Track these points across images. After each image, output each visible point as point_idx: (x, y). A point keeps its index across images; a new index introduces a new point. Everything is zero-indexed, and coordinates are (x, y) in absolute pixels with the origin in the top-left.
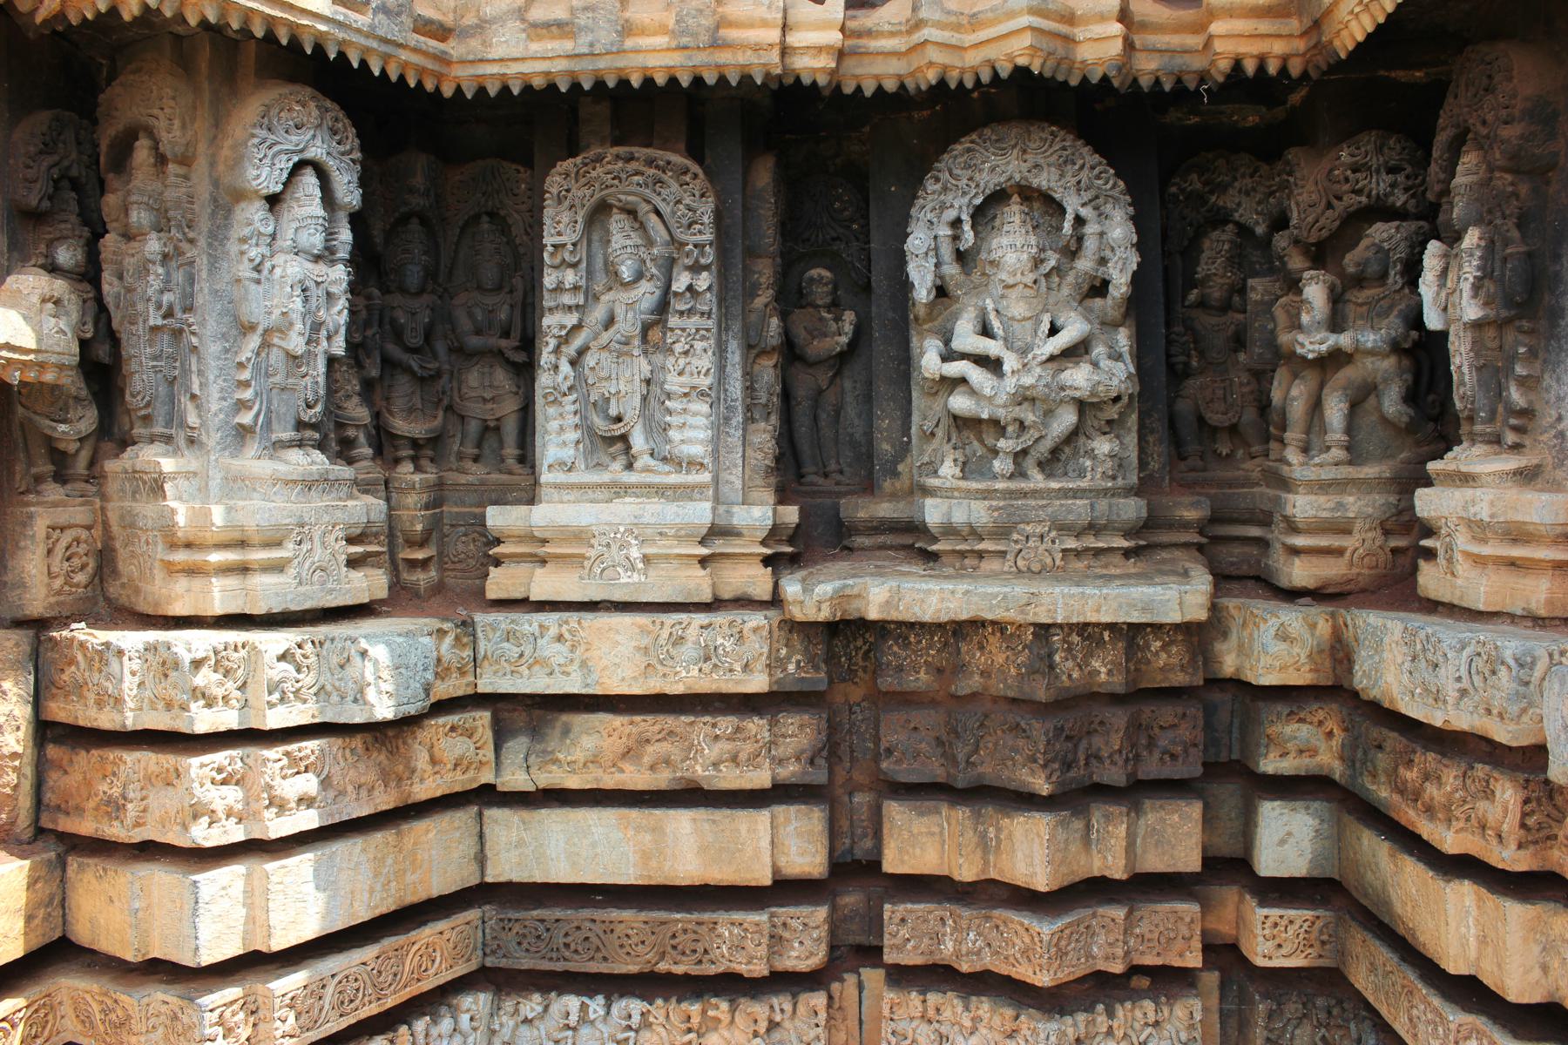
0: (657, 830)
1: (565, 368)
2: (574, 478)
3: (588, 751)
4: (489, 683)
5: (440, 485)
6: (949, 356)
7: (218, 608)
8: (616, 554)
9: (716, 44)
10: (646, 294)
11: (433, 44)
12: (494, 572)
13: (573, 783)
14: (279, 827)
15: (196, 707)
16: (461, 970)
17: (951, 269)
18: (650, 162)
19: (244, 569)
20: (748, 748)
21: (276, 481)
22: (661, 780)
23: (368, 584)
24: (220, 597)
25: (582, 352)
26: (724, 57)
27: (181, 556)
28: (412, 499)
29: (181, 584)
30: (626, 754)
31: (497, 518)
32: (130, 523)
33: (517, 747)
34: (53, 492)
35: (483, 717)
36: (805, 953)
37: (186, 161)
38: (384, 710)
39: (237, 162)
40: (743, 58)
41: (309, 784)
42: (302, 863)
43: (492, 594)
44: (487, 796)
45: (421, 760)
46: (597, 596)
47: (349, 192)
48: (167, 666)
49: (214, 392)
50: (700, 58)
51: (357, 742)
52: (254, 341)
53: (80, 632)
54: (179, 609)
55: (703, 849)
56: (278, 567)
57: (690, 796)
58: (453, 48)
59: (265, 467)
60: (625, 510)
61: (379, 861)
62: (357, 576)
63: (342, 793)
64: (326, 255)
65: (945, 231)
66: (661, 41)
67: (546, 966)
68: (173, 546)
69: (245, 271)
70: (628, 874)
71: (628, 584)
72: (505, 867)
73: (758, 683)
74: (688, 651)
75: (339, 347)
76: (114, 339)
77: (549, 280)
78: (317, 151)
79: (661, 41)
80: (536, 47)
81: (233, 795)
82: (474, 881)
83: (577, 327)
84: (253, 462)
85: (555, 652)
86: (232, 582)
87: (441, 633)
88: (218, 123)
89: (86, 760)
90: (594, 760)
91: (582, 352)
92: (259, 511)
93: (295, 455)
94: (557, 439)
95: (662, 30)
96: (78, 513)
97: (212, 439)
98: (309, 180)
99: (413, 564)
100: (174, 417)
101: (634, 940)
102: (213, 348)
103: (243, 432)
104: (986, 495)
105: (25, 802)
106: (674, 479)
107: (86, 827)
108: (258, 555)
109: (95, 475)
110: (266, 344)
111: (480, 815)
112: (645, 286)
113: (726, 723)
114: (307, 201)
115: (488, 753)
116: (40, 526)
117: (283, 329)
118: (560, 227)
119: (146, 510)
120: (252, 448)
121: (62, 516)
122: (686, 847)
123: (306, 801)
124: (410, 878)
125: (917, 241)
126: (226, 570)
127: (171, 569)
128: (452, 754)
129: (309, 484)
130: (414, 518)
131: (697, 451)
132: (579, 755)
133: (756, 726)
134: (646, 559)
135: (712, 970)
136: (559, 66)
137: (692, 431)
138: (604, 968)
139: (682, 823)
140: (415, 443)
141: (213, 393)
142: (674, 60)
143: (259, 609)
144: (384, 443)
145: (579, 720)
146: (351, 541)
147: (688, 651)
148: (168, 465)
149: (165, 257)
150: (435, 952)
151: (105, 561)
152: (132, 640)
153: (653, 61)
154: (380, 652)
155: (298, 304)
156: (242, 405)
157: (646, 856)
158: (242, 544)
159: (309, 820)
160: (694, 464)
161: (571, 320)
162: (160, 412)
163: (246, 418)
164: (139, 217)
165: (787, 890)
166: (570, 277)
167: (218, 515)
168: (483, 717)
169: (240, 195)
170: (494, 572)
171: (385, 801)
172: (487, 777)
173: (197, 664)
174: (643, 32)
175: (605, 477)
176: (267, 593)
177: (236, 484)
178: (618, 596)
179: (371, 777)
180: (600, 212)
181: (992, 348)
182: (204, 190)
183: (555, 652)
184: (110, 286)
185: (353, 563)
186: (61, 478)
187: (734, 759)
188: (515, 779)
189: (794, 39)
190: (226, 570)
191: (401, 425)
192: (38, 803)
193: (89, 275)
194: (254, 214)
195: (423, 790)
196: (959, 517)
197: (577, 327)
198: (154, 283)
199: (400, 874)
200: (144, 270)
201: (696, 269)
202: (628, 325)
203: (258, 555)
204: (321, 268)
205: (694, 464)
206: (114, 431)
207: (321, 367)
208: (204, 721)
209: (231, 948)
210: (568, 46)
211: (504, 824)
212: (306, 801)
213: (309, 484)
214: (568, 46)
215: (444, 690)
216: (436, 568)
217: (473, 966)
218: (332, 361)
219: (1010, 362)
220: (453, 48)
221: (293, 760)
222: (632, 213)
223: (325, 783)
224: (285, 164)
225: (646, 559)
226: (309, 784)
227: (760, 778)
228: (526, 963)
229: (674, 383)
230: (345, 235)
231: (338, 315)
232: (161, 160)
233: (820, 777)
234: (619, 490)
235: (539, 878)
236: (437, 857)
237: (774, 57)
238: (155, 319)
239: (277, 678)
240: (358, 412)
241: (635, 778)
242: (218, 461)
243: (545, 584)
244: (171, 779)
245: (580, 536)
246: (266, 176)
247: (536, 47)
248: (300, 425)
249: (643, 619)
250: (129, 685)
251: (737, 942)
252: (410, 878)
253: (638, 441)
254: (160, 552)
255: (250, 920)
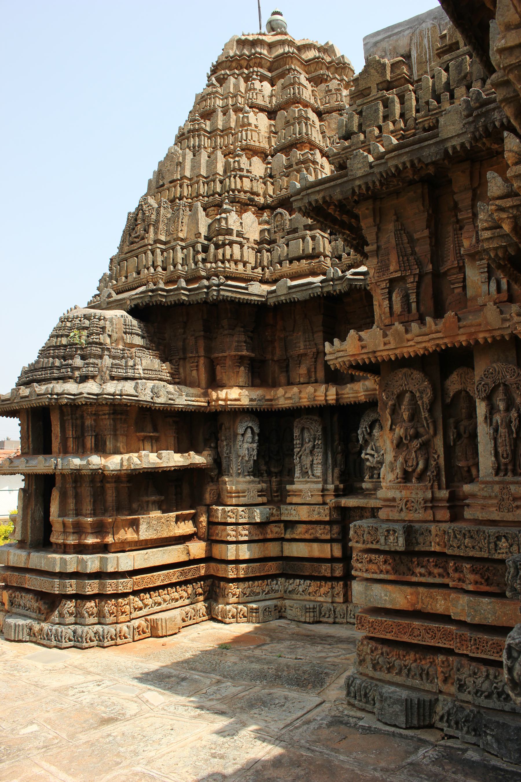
0: (311, 547)
1: (298, 459)
2: (299, 480)
3: (300, 531)
4: (284, 518)
5: (281, 481)
6: (367, 454)
7: (234, 503)
8: (307, 494)
9: (315, 400)
10: (310, 445)
11: (269, 403)
12: (288, 498)
13: (297, 537)
14: (241, 539)
15: (228, 518)
16: (278, 572)
17: (367, 437)
18: (311, 419)
19: (239, 497)
20: (326, 531)
21: (244, 482)
22: (311, 537)
23: (260, 500)
24: (234, 501)
25: (301, 456)
26: (316, 403)
27: (229, 495)
28: (274, 484)
29: (229, 499)
30: (306, 532)
31: (288, 487)
32: (222, 489)
33: (289, 531)
34: (211, 484)
35: (282, 525)
36: (338, 573)
37: (229, 428)
38: (258, 520)
39: (237, 429)
40: (319, 403)
41: (247, 532)
42: (245, 545)
43: (288, 502)
44: (283, 540)
45: (269, 531)
46: (303, 502)
47: (257, 430)
48: (224, 511)
49: (234, 467)
50: (312, 403)
51: (256, 526)
52: (241, 458)
53: (214, 507)
54: (229, 503)
55: (319, 551)
56: (245, 496)
57: (316, 540)
58: (273, 403)
59: (244, 479)
60: (308, 486)
61: (260, 548)
62: (260, 498)
63: (253, 535)
64: (253, 442)
65: (364, 429)
66: (306, 400)
67: (293, 573)
68: (228, 493)
69: (238, 447)
70: (306, 555)
71: (309, 500)
72: (286, 553)
73: (327, 519)
74: (316, 512)
75: (255, 458)
76: (220, 458)
77: (295, 442)
78: (250, 425)
79: (306, 400)
80: (286, 402)
81: (234, 533)
82: (281, 555)
83: (300, 451)
84: (241, 479)
85: (294, 512)
86: (237, 499)
87: (273, 509)
88: (234, 422)
89: (214, 527)
90: (300, 533)
91: (301, 456)
92: (241, 487)
93: (248, 477)
94: (297, 474)
95: (306, 398)
96: (215, 487)
97: (234, 475)
98: (249, 430)
99: (275, 496)
100: (229, 471)
101: (307, 569)
102: (234, 460)
103: (239, 474)
104: (372, 482)
105: (206, 534)
106: (316, 480)
107: (214, 538)
108: (241, 494)
109: (218, 481)
110: (242, 459)
111: (282, 543)
112: (311, 443)
113: (322, 527)
114: (249, 434)
115: (283, 531)
116: (208, 490)
117: (245, 456)
118: (296, 433)
119: (224, 487)
120: (241, 476)
121: (212, 488)
122: (316, 550)
123: (245, 535)
124: (266, 552)
125: (359, 432)
126: (235, 497)
127: (228, 497)
128: (273, 531)
129: (250, 482)
130: (274, 487)
131: (319, 474)
132: (298, 532)
133: (328, 527)
134: (312, 495)
135: (321, 575)
136: (290, 405)
137: (318, 471)
138: (302, 574)
139: (315, 545)
140: (275, 473)
141: (234, 468)
142: (308, 403)
143: (241, 503)
144: (270, 474)
145: (299, 525)
146: (258, 492)
147: (316, 512)
148: (227, 479)
149: (227, 445)
150: (272, 568)
151: (219, 496)
152: (220, 508)
153: (305, 404)
154: (258, 511)
155: (247, 452)
156: (239, 469)
157: (309, 552)
158: (239, 493)
159: (246, 538)
160: (318, 477)
161: (299, 450)
162: (227, 470)
163: (239, 471)
164: (223, 438)
165: (333, 560)
166: (298, 442)
167: (234, 488)
168: (282, 525)
169: (238, 434)
170: (288, 498)
171: (261, 537)
172: (283, 536)
173: (229, 512)
174: (303, 398)
175: (304, 480)
176: (242, 500)
177: (238, 483)
178: (307, 502)
179: (258, 533)
180: (302, 430)
181: (372, 452)
182: (232, 434)
183: (294, 512)
184: (219, 450)
185: (259, 496)
186: (212, 481)
187: (324, 533)
188: (288, 536)
189: (328, 398)
190: (235, 497)
191: (273, 470)
192: (208, 535)
193: (216, 447)
194: (240, 438)
195: (269, 536)
196: (367, 487)
197: (300, 451)
198: (225, 449)
199: (264, 551)
200: (223, 447)
201: (319, 439)
202: (308, 451)
203: (241, 494)
204: (252, 445)
205: (318, 477)
206: (221, 473)
207: (252, 462)
208: (229, 520)
209: (233, 558)
210: (291, 401)
211: (286, 545)
212: (245, 535)
213: (250, 482)
214: (291, 401)
215: (273, 519)
216: (276, 496)
217: (281, 572)
218: (254, 461)
219: (376, 456)
220: (273, 403)
221: (244, 528)
222: (308, 429)
223: (250, 533)
224: (244, 428)
225: (312, 495)
226: (247, 532)
227: (328, 537)
228: (290, 572)
229: (315, 462)
230: (257, 438)
231: (255, 452)
232: (226, 429)
233: (340, 537)
234: (307, 482)
235: (292, 555)
236: (273, 550)
237: (324, 402)
238: (225, 455)
239: (242, 514)
240: (264, 468)
241: (307, 536)
242: (235, 479)
243: (295, 500)
244: (225, 530)
245: (301, 491)
246: (241, 431)
247: (286, 402)
248: (248, 472)
249: (308, 506)
250: (220, 515)
251: (325, 570)
252: (266, 552)
253: (310, 473)
254: (226, 494)
255: (236, 554)
